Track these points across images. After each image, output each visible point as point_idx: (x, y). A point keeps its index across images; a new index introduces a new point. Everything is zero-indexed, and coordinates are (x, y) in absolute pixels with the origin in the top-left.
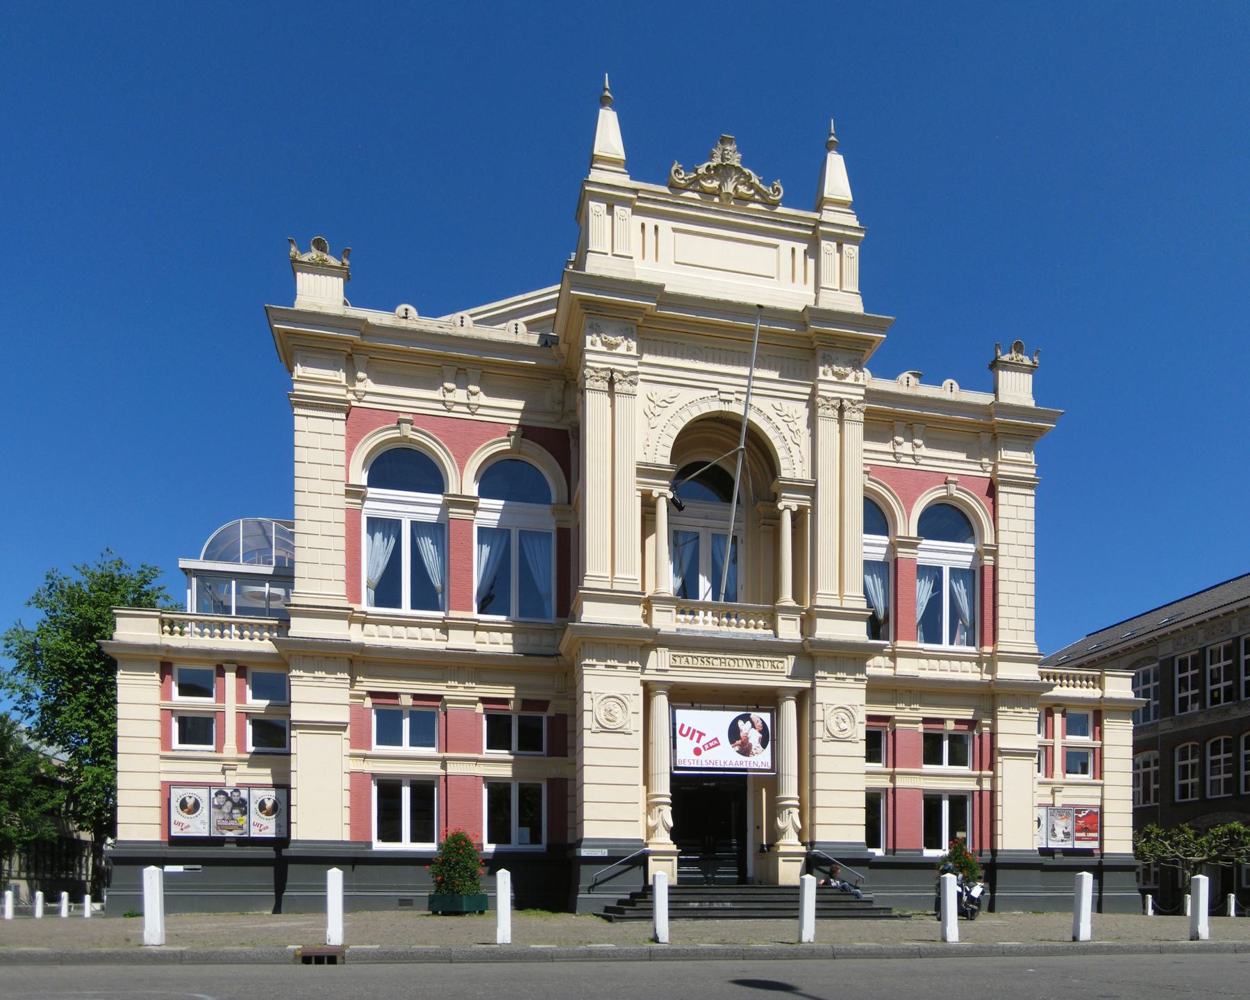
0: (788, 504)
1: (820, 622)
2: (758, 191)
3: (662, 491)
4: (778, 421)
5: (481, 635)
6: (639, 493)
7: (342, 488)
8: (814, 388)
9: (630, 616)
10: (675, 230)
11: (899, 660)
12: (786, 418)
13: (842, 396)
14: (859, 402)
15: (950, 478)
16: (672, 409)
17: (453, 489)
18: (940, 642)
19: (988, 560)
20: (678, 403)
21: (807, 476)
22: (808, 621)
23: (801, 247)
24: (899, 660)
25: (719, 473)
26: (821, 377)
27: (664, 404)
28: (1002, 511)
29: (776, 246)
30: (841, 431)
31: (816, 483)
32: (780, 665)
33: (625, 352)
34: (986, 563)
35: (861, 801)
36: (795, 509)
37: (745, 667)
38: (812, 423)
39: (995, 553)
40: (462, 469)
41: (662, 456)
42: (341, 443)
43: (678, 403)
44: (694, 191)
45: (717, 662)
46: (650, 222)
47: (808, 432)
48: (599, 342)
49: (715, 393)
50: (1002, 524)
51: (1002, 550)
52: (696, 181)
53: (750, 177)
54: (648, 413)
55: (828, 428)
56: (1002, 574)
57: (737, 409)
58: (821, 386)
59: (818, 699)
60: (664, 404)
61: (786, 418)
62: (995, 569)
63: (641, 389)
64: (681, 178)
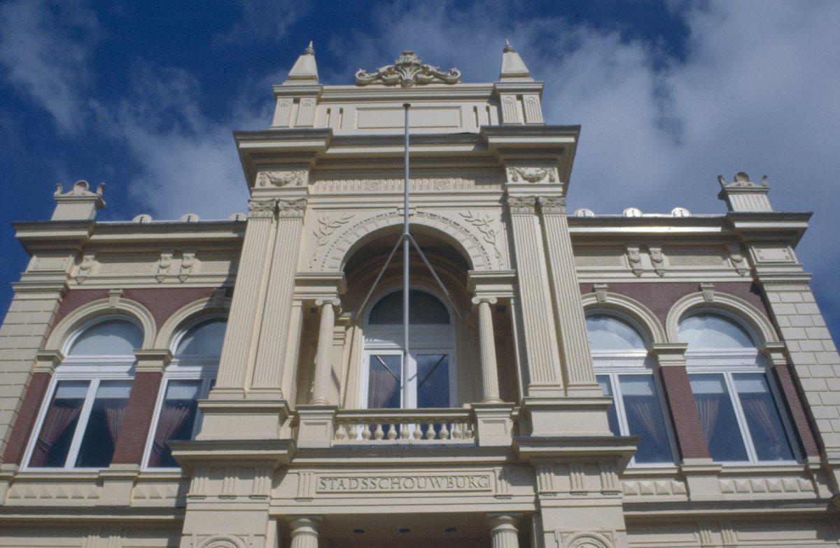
0: (485, 297)
1: (536, 417)
2: (437, 76)
3: (328, 298)
4: (468, 226)
5: (143, 488)
6: (300, 303)
7: (33, 354)
8: (505, 187)
9: (267, 428)
10: (358, 109)
11: (690, 480)
12: (477, 223)
13: (537, 195)
14: (560, 197)
15: (112, 291)
16: (344, 228)
17: (147, 344)
18: (746, 458)
19: (778, 359)
20: (352, 222)
21: (506, 266)
22: (522, 424)
23: (482, 105)
24: (690, 480)
25: (405, 282)
26: (510, 181)
27: (338, 225)
28: (776, 309)
29: (458, 107)
30: (542, 222)
31: (516, 273)
32: (483, 482)
33: (296, 186)
34: (776, 362)
35: (24, 379)
36: (494, 301)
37: (430, 488)
38: (506, 218)
39: (784, 351)
40: (159, 328)
41: (333, 265)
42: (47, 318)
43: (352, 222)
44: (378, 84)
45: (386, 484)
46: (335, 107)
47: (503, 225)
48: (268, 180)
49: (395, 210)
50: (781, 321)
51: (791, 346)
52: (379, 77)
53: (428, 68)
54: (318, 233)
55: (525, 223)
56: (800, 372)
57: (400, 220)
58: (510, 190)
59: (546, 526)
60: (338, 225)
61: (477, 223)
62: (790, 367)
63: (311, 216)
64: (367, 77)
